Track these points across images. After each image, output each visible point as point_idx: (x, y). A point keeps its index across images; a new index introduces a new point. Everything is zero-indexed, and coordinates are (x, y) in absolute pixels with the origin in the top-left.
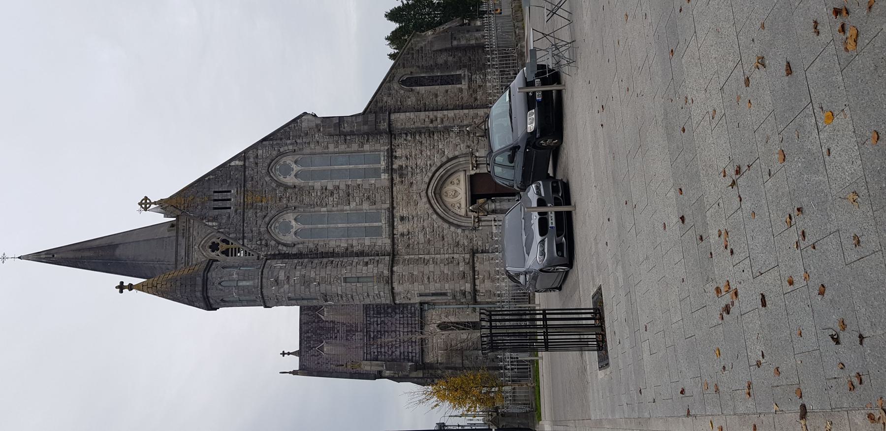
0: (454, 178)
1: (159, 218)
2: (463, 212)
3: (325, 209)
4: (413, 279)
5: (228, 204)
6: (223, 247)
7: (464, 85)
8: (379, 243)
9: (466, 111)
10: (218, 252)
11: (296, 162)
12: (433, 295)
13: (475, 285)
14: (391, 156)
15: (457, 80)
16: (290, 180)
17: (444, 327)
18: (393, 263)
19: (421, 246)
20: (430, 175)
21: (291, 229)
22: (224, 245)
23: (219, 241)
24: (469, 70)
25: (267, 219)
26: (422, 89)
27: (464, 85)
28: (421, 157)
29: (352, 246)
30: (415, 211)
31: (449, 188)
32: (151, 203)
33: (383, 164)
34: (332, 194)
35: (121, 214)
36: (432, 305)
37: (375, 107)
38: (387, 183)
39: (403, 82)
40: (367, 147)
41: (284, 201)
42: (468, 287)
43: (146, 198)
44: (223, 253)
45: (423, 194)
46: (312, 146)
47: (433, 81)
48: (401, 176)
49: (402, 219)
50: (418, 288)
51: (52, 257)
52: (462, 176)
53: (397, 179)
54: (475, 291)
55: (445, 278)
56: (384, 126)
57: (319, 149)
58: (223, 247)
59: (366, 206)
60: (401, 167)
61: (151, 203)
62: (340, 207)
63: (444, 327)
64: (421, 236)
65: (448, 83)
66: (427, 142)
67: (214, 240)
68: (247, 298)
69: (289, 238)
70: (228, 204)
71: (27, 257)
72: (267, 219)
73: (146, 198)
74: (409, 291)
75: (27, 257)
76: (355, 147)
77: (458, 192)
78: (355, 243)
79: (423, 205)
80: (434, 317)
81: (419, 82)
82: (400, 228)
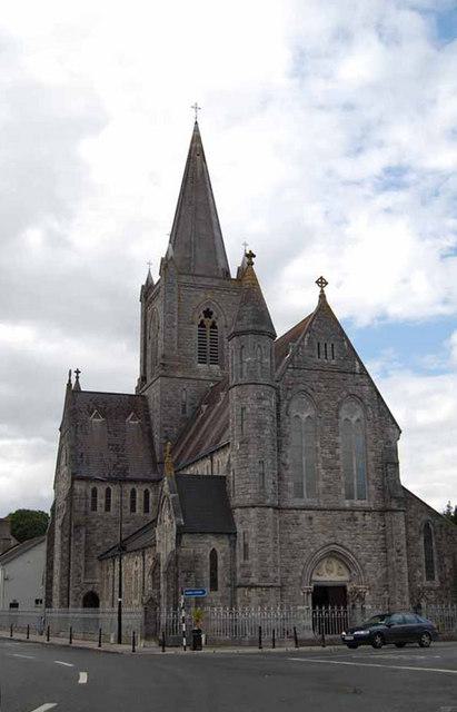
0: (344, 570)
1: (234, 263)
2: (315, 577)
3: (318, 445)
4: (261, 527)
5: (323, 356)
6: (208, 322)
7: (427, 583)
8: (290, 496)
9: (407, 584)
10: (203, 318)
11: (358, 420)
12: (246, 545)
13: (256, 587)
14: (366, 511)
15: (430, 577)
16: (343, 414)
17: (214, 554)
18: (276, 508)
19: (286, 536)
20: (349, 547)
21: (302, 412)
22: (210, 324)
23: (214, 318)
24: (440, 588)
25: (310, 391)
26: (421, 543)
27: (427, 583)
28: (361, 540)
29: (287, 469)
30: (313, 533)
31: (335, 565)
32: (322, 287)
33: (358, 503)
34: (331, 453)
35: (241, 227)
36: (233, 544)
37: (409, 498)
38: (342, 506)
39: (427, 526)
40: (372, 487)
41: (326, 408)
42: (254, 580)
43: (327, 283)
44: (202, 322)
45: (332, 540)
46: (373, 437)
47: (429, 552)
48: (349, 519)
49: (311, 518)
50: (253, 530)
51: (196, 155)
52: (346, 577)
53: (347, 515)
54: (251, 587)
55: (263, 558)
56: (394, 505)
57: (370, 442)
58: (208, 322)
59: (321, 484)
60: (356, 519)
61: (322, 287)
62: (321, 459)
63: (214, 554)
64: (295, 536)
65: (427, 568)
66: (378, 544)
67: (215, 313)
68: (245, 370)
69: (293, 412)
70: (323, 356)
71: (196, 130)
72: (310, 391)
73: (327, 283)
74: (247, 523)
75: (196, 130)
76: (373, 476)
77: (332, 575)
78: (290, 472)
79: (324, 539)
80: (221, 546)
81: (428, 540)
82: (303, 515)
